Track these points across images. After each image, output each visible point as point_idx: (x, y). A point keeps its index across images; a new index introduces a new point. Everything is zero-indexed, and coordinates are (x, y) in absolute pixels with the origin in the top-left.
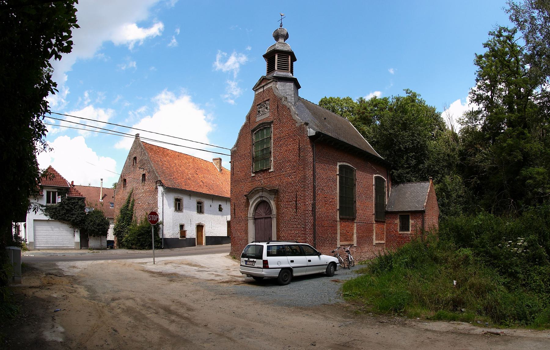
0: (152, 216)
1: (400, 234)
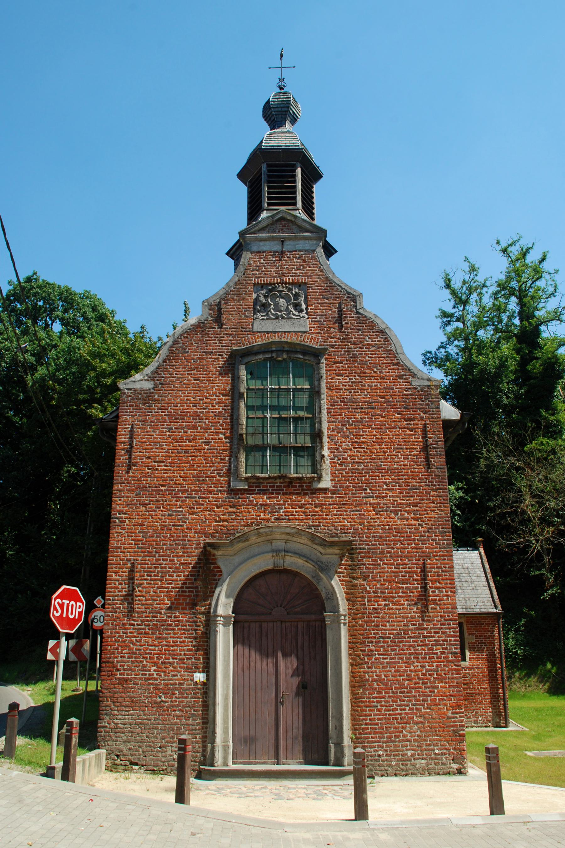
0: (66, 602)
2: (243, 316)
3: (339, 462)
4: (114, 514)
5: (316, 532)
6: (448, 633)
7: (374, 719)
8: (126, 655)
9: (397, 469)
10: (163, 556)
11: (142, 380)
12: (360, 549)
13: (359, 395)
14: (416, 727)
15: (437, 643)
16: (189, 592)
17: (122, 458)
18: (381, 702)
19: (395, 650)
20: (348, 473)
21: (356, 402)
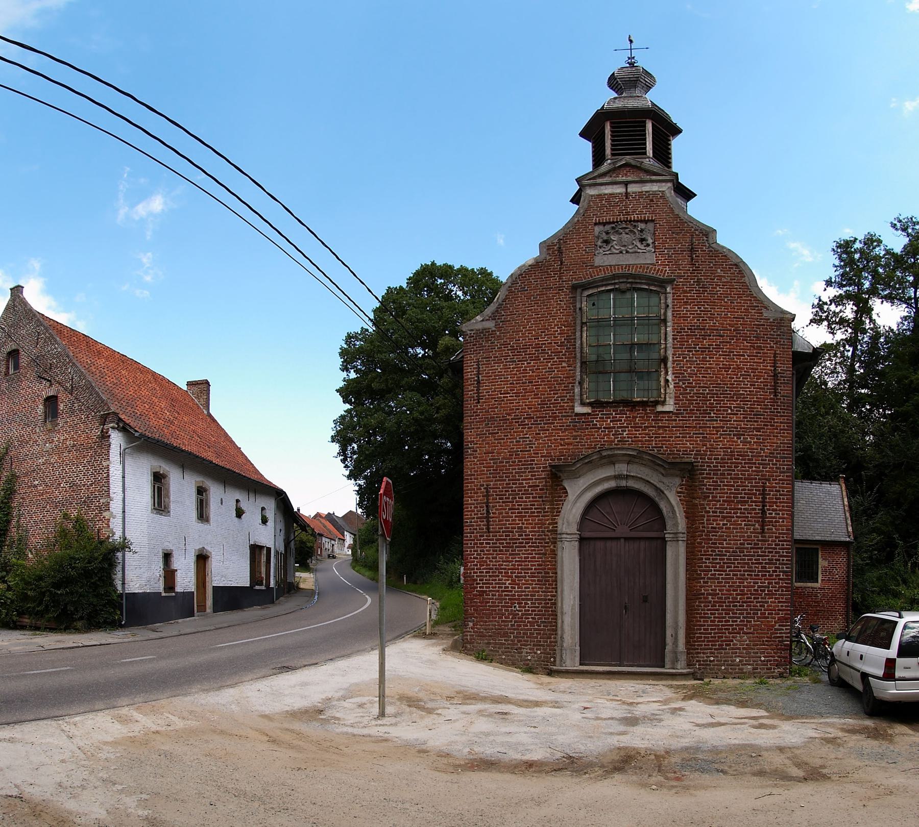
1: (797, 588)
2: (584, 252)
3: (683, 386)
4: (466, 445)
5: (659, 454)
6: (781, 554)
7: (707, 629)
8: (485, 571)
9: (744, 394)
10: (513, 480)
11: (483, 320)
12: (702, 470)
13: (707, 323)
14: (746, 637)
15: (770, 562)
16: (537, 512)
17: (470, 393)
18: (715, 614)
19: (731, 567)
20: (693, 397)
21: (704, 329)
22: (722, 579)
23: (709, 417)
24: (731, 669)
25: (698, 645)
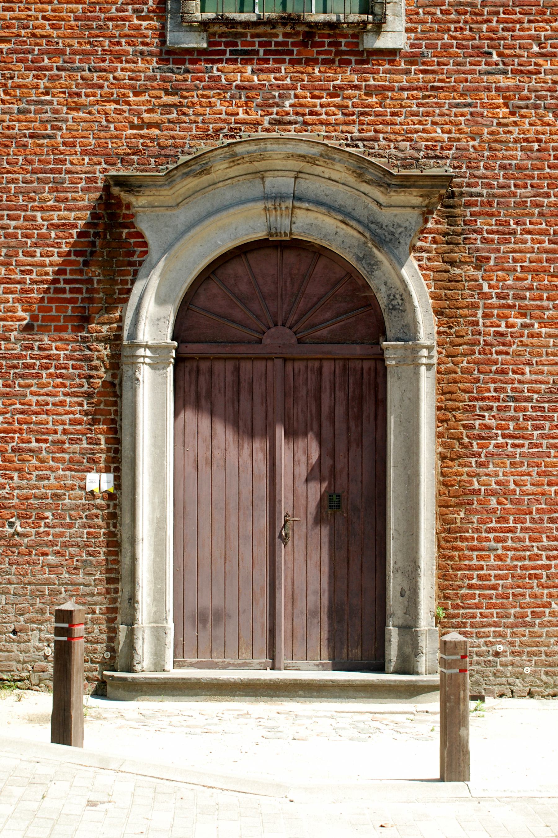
16: (72, 291)
22: (523, 455)
23: (487, 64)
24: (547, 673)
25: (465, 616)
